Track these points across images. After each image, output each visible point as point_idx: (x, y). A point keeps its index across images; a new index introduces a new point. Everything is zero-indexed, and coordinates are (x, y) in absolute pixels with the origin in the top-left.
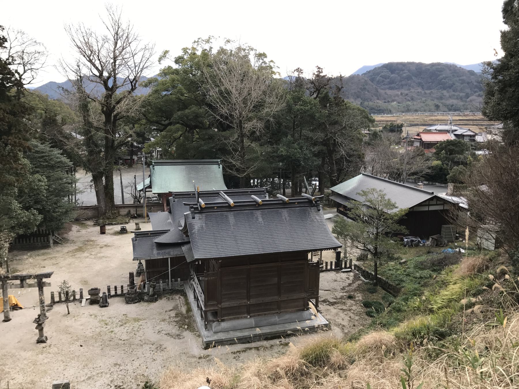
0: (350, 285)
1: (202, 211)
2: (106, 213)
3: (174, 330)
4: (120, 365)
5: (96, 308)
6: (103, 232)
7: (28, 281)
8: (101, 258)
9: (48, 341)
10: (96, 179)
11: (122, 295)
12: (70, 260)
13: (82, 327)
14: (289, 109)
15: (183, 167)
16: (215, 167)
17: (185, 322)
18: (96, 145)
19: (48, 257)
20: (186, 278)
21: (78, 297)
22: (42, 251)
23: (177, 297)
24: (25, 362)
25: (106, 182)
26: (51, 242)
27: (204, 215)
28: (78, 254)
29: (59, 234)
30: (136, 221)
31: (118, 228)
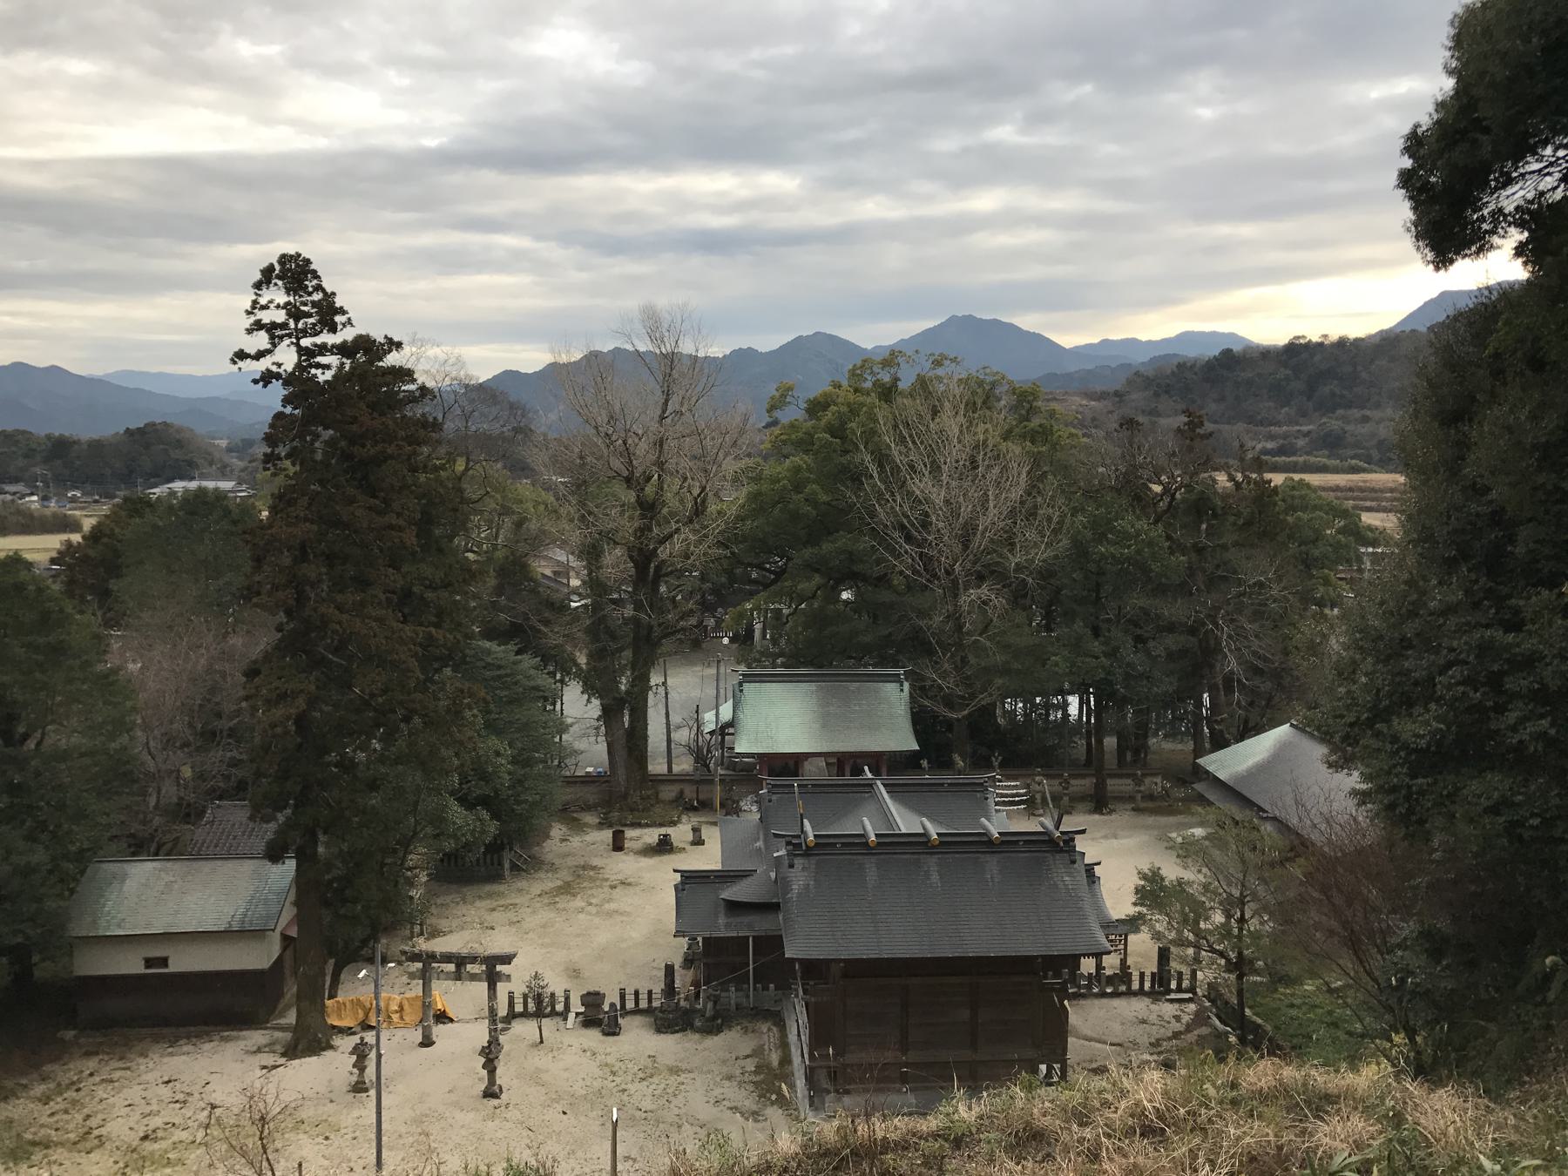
0: (1176, 1035)
1: (808, 852)
2: (630, 795)
3: (750, 1103)
4: (634, 1160)
5: (593, 1037)
6: (618, 845)
7: (469, 967)
8: (610, 914)
9: (503, 1096)
10: (609, 714)
11: (649, 1011)
12: (545, 915)
13: (566, 1075)
14: (1080, 551)
15: (813, 686)
16: (891, 687)
17: (768, 1084)
18: (613, 637)
19: (501, 902)
20: (785, 987)
21: (560, 1007)
22: (488, 888)
23: (764, 1028)
24: (464, 1133)
25: (631, 722)
26: (507, 865)
27: (813, 860)
28: (563, 902)
29: (522, 847)
30: (695, 819)
31: (651, 836)
